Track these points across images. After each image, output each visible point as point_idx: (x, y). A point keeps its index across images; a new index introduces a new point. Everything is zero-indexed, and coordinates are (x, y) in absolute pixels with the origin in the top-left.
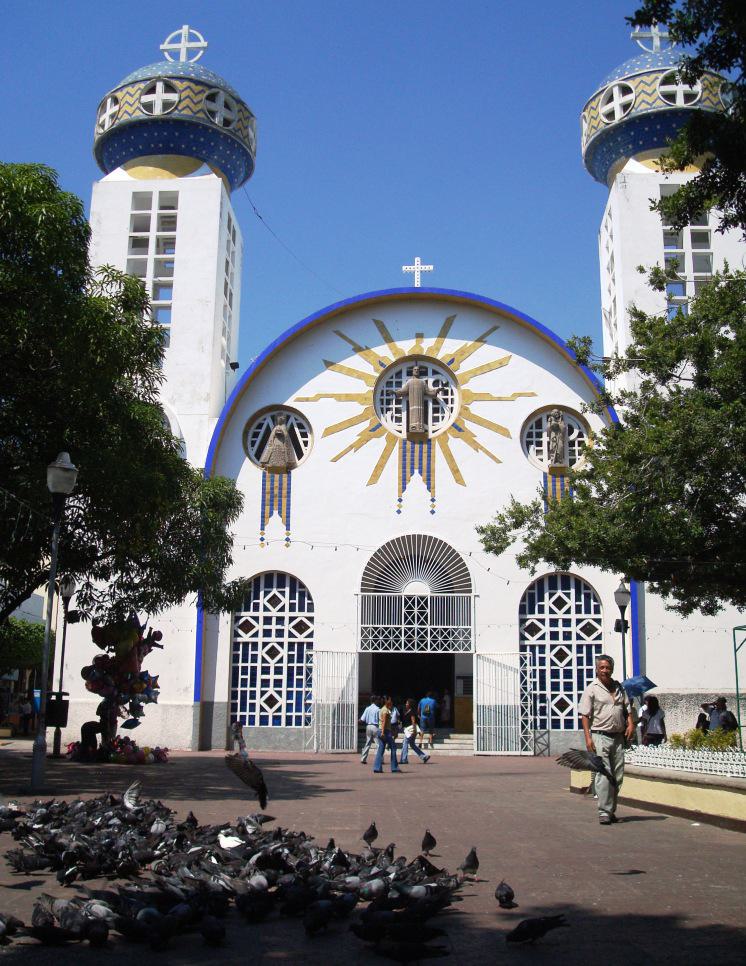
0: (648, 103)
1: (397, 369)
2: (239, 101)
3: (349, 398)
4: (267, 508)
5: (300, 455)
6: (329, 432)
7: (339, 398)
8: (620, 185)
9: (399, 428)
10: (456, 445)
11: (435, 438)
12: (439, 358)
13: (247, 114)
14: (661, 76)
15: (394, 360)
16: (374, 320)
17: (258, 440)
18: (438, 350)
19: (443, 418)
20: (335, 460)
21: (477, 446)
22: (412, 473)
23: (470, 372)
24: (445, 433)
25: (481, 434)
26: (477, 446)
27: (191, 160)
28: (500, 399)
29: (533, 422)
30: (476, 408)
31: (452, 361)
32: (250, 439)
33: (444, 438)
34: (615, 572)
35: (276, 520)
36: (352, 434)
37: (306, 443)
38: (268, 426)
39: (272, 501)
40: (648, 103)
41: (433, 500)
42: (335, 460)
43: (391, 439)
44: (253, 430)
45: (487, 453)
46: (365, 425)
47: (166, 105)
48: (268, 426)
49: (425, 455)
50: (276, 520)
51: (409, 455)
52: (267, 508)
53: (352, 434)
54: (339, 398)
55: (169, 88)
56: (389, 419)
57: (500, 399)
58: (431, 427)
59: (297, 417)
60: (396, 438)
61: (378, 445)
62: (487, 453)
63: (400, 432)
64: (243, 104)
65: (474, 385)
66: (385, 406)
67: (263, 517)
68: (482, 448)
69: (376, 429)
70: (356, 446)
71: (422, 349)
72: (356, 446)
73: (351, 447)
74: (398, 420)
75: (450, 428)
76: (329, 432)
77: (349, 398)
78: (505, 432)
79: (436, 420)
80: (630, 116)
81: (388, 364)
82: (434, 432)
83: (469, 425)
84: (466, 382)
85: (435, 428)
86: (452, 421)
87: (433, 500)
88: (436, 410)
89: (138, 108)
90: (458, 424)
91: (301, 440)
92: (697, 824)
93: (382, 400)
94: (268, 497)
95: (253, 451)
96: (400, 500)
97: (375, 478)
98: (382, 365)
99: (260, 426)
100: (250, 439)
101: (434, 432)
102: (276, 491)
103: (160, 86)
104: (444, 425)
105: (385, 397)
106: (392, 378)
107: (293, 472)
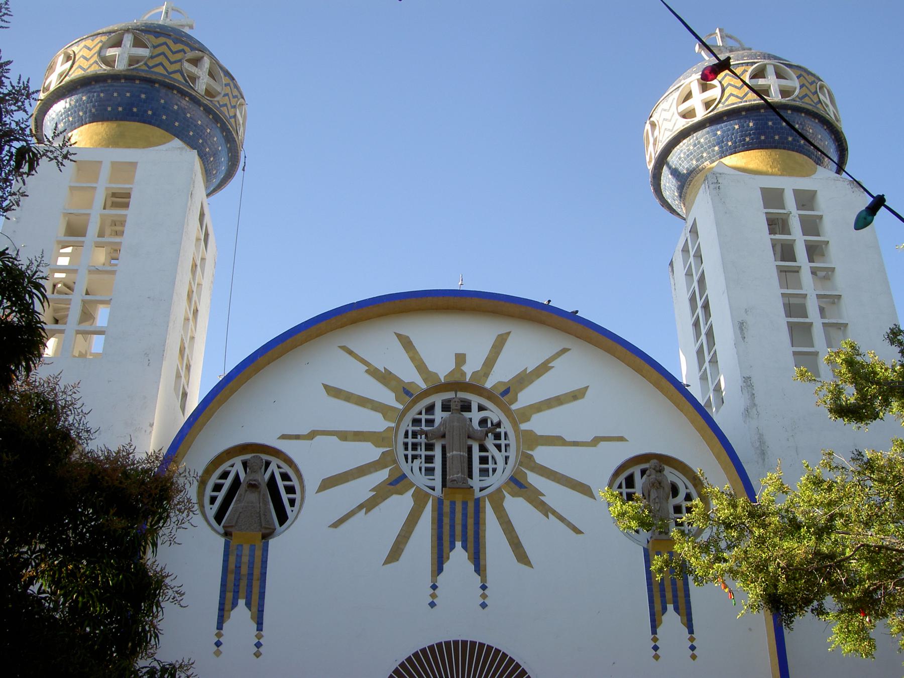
0: (737, 97)
1: (427, 402)
2: (227, 74)
3: (359, 436)
4: (230, 595)
5: (283, 518)
6: (328, 484)
7: (344, 436)
8: (712, 186)
9: (431, 484)
10: (515, 506)
11: (484, 497)
12: (489, 385)
13: (236, 93)
14: (751, 69)
15: (448, 455)
16: (399, 336)
17: (221, 495)
18: (486, 375)
19: (494, 470)
20: (336, 525)
21: (545, 509)
22: (452, 547)
23: (531, 406)
24: (499, 490)
25: (551, 492)
26: (545, 509)
27: (158, 132)
28: (575, 444)
29: (622, 478)
30: (542, 455)
31: (506, 392)
32: (209, 492)
33: (497, 501)
34: (401, 493)
35: (241, 614)
36: (363, 488)
37: (292, 502)
38: (237, 476)
39: (237, 585)
40: (737, 97)
41: (484, 587)
42: (336, 525)
43: (420, 499)
44: (214, 480)
45: (562, 519)
46: (383, 475)
47: (133, 60)
48: (237, 476)
49: (471, 521)
50: (241, 614)
51: (446, 520)
52: (230, 595)
53: (363, 488)
54: (344, 436)
55: (138, 43)
56: (416, 470)
57: (575, 444)
58: (476, 482)
59: (282, 464)
60: (427, 495)
61: (402, 504)
62: (562, 519)
63: (433, 489)
64: (233, 79)
65: (539, 424)
66: (410, 453)
67: (222, 609)
68: (554, 513)
69: (398, 483)
70: (369, 505)
71: (464, 374)
72: (369, 505)
73: (360, 507)
74: (430, 471)
75: (507, 483)
76: (328, 484)
77: (359, 436)
78: (585, 490)
79: (484, 472)
80: (715, 112)
81: (416, 393)
82: (481, 490)
83: (533, 479)
84: (527, 419)
85: (484, 484)
86: (508, 474)
87: (484, 587)
88: (484, 460)
89: (96, 62)
90: (517, 477)
91: (285, 497)
92: (222, 176)
93: (406, 444)
94: (231, 577)
95: (212, 511)
96: (434, 587)
97: (395, 554)
98: (407, 393)
99: (225, 475)
100: (209, 492)
101: (481, 490)
102: (244, 570)
103: (128, 40)
104: (496, 481)
105: (410, 440)
106: (420, 413)
107: (272, 542)
